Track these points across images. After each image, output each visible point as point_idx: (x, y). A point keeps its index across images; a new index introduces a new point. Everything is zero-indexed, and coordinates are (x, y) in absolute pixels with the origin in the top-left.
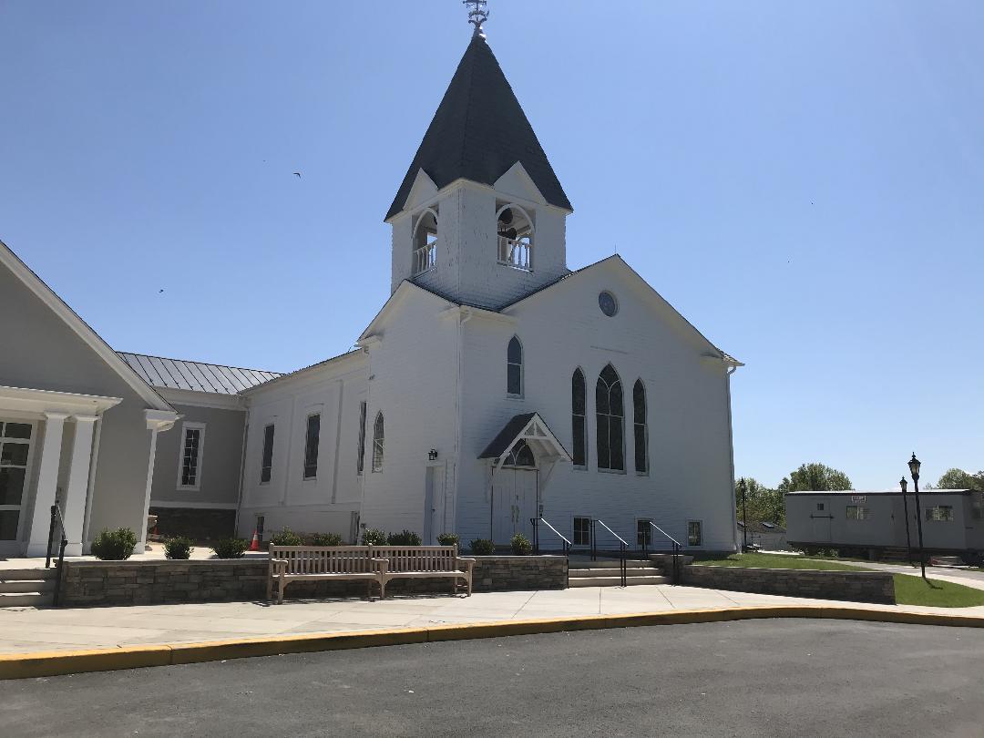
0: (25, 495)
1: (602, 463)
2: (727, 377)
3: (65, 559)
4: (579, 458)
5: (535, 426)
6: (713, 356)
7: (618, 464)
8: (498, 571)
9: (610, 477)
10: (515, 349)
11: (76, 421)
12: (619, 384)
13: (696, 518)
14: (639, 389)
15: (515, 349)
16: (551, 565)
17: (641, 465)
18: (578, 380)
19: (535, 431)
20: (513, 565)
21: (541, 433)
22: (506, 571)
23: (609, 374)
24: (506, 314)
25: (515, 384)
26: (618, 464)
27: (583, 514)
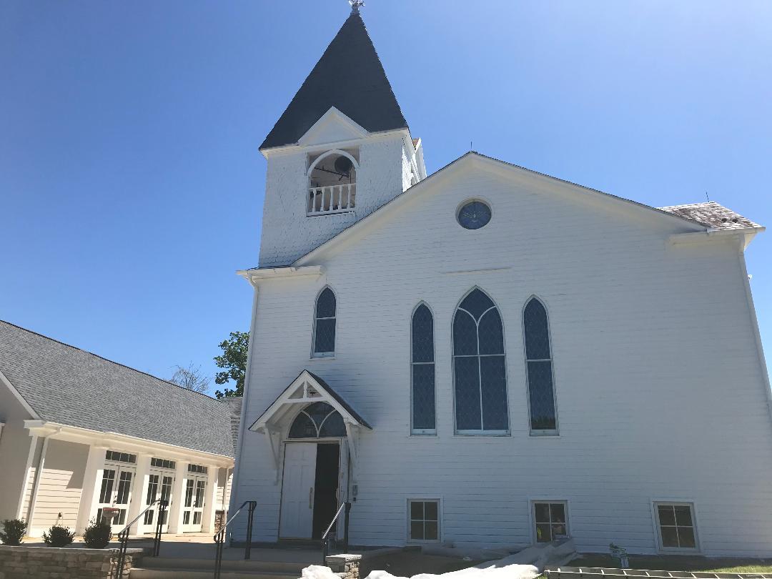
0: (410, 506)
1: (465, 419)
2: (739, 257)
3: (223, 562)
4: (423, 415)
5: (305, 387)
6: (697, 231)
7: (498, 419)
8: (13, 564)
9: (481, 442)
10: (326, 302)
11: (29, 430)
12: (495, 311)
13: (676, 497)
14: (535, 315)
15: (326, 302)
16: (85, 562)
17: (543, 418)
18: (422, 319)
19: (305, 392)
20: (34, 559)
21: (313, 393)
22: (23, 565)
23: (477, 301)
24: (305, 265)
25: (325, 337)
26: (498, 419)
27: (424, 496)
